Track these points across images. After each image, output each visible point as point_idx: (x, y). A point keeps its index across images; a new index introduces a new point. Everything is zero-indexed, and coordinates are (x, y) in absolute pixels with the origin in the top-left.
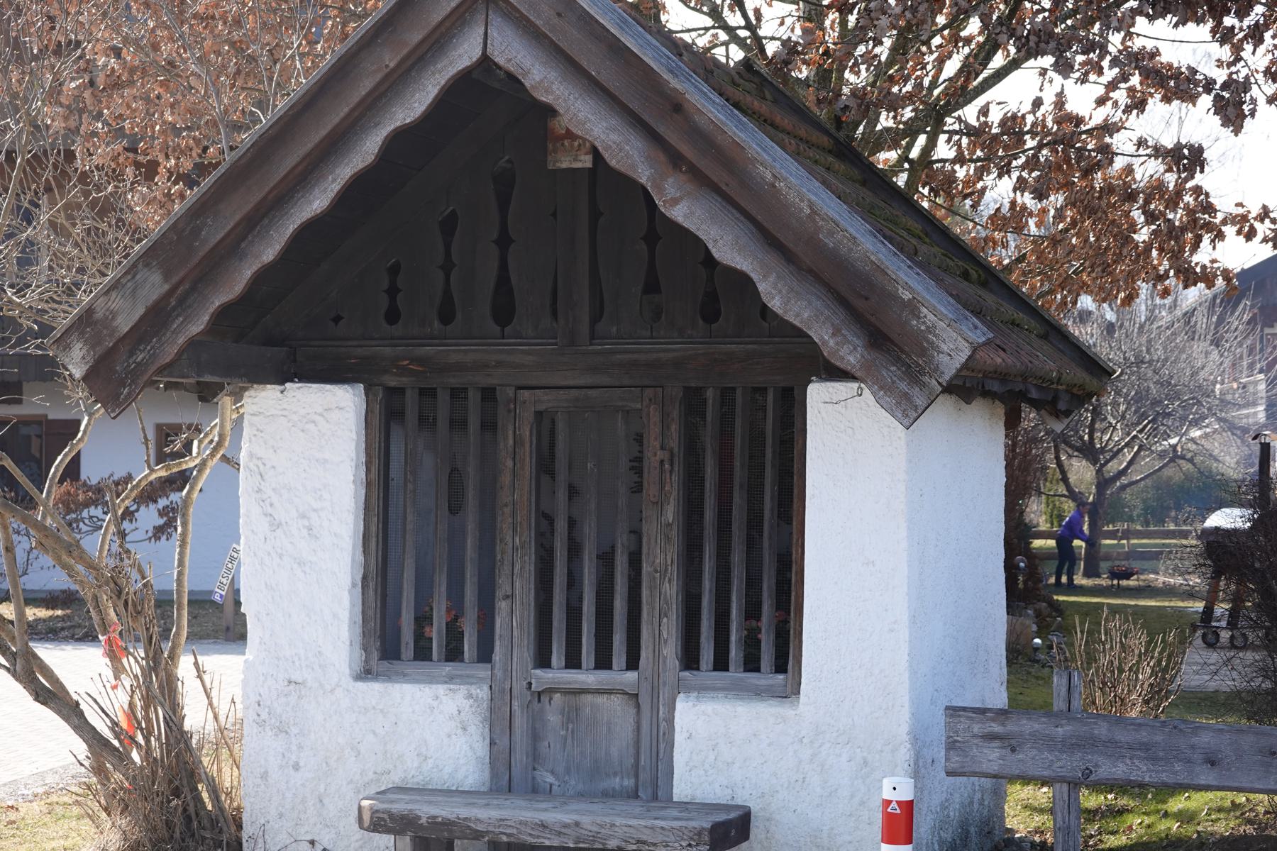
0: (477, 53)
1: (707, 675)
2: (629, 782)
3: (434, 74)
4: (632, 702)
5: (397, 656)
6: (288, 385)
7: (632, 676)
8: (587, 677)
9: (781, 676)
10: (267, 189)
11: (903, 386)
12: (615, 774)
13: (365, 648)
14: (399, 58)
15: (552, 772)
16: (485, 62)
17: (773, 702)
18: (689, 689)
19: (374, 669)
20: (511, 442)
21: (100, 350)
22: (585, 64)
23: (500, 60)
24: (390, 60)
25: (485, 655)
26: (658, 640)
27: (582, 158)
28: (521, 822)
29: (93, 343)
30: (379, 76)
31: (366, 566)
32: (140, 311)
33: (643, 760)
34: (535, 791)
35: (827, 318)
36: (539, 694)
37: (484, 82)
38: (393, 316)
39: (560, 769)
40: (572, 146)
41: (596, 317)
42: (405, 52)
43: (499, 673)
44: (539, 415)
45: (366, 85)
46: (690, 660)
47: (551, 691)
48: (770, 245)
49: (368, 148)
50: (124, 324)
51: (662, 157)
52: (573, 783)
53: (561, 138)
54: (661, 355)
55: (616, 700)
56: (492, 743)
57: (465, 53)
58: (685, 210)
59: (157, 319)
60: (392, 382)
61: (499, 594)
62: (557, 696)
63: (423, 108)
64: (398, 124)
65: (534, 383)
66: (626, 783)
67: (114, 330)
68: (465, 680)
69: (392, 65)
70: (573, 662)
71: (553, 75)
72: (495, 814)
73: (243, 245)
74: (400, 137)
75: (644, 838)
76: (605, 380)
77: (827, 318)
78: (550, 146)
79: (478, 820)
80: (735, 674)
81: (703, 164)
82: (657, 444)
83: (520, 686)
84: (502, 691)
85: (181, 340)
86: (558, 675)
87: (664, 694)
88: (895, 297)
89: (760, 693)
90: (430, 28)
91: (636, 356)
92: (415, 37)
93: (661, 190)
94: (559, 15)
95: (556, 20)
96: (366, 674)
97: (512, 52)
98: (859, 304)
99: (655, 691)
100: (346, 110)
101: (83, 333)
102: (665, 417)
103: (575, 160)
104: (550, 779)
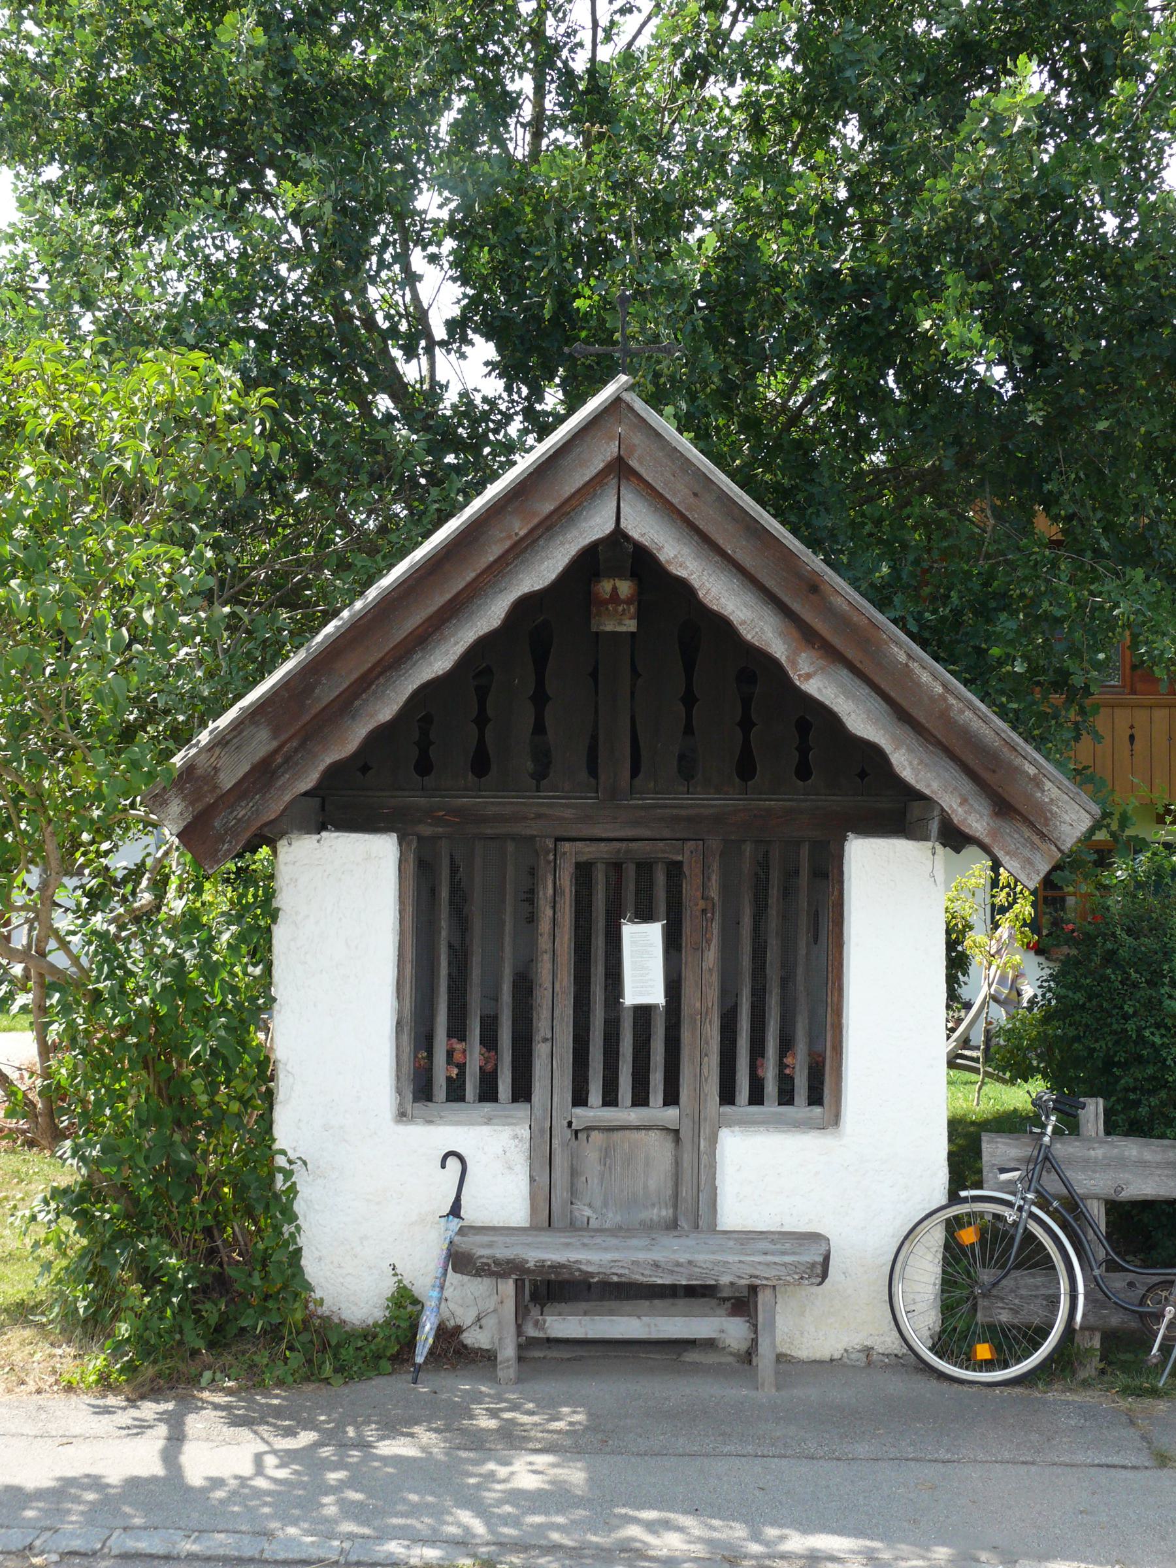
0: (609, 527)
1: (742, 1107)
2: (667, 1213)
3: (562, 544)
4: (670, 1137)
5: (462, 1099)
6: (324, 834)
7: (672, 1112)
8: (625, 1114)
9: (817, 1110)
10: (387, 649)
11: (1027, 852)
12: (653, 1205)
13: (399, 1091)
14: (530, 526)
15: (590, 1206)
16: (619, 535)
17: (816, 1133)
18: (730, 1124)
19: (409, 1112)
20: (550, 891)
21: (200, 806)
22: (720, 542)
23: (635, 534)
24: (520, 528)
25: (522, 1093)
26: (700, 1078)
27: (627, 622)
28: (633, 1262)
29: (191, 800)
30: (508, 544)
31: (400, 1012)
32: (245, 768)
33: (684, 1192)
34: (573, 1226)
35: (955, 789)
36: (576, 1132)
37: (620, 554)
38: (424, 767)
39: (598, 1203)
40: (616, 611)
41: (635, 772)
42: (536, 521)
43: (538, 1112)
44: (578, 865)
45: (494, 552)
46: (727, 1096)
47: (588, 1129)
48: (900, 719)
49: (491, 615)
50: (227, 781)
51: (796, 634)
52: (611, 1215)
53: (606, 602)
54: (702, 810)
55: (654, 1136)
56: (532, 1179)
57: (596, 525)
58: (822, 685)
59: (264, 774)
60: (426, 830)
61: (537, 1037)
62: (595, 1135)
63: (554, 576)
64: (526, 590)
65: (573, 834)
66: (664, 1213)
67: (216, 787)
68: (506, 1121)
69: (522, 533)
70: (610, 1100)
71: (686, 551)
72: (609, 1256)
73: (357, 703)
74: (524, 605)
75: (757, 1273)
76: (647, 833)
77: (955, 789)
78: (594, 610)
79: (589, 1262)
80: (771, 1108)
81: (836, 641)
82: (699, 894)
83: (560, 1125)
84: (542, 1131)
85: (288, 797)
86: (595, 1112)
87: (706, 1130)
88: (1018, 770)
89: (798, 1125)
90: (562, 499)
91: (675, 811)
92: (548, 507)
93: (794, 663)
94: (695, 495)
95: (692, 500)
96: (402, 1115)
97: (644, 526)
98: (986, 775)
99: (697, 1124)
100: (473, 575)
101: (181, 789)
102: (705, 868)
103: (620, 624)
104: (588, 1212)
